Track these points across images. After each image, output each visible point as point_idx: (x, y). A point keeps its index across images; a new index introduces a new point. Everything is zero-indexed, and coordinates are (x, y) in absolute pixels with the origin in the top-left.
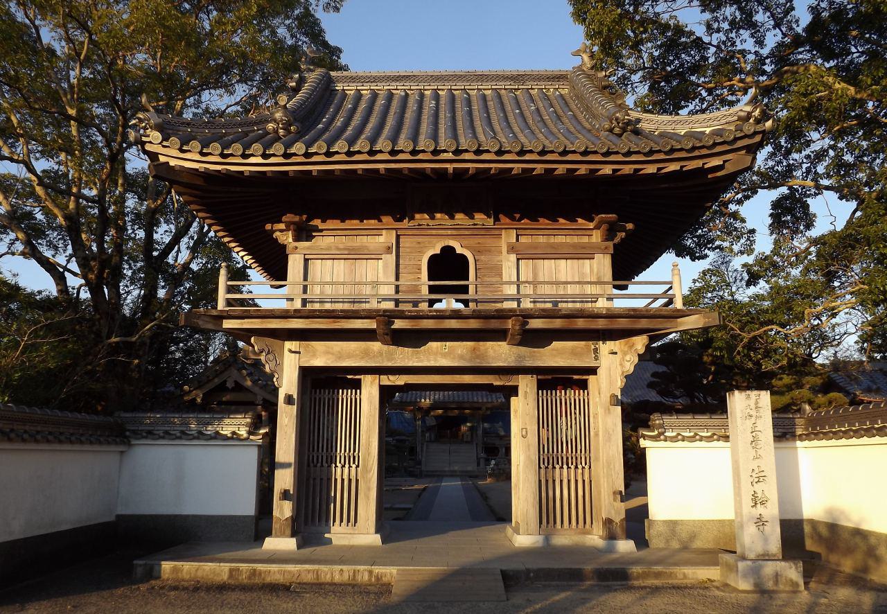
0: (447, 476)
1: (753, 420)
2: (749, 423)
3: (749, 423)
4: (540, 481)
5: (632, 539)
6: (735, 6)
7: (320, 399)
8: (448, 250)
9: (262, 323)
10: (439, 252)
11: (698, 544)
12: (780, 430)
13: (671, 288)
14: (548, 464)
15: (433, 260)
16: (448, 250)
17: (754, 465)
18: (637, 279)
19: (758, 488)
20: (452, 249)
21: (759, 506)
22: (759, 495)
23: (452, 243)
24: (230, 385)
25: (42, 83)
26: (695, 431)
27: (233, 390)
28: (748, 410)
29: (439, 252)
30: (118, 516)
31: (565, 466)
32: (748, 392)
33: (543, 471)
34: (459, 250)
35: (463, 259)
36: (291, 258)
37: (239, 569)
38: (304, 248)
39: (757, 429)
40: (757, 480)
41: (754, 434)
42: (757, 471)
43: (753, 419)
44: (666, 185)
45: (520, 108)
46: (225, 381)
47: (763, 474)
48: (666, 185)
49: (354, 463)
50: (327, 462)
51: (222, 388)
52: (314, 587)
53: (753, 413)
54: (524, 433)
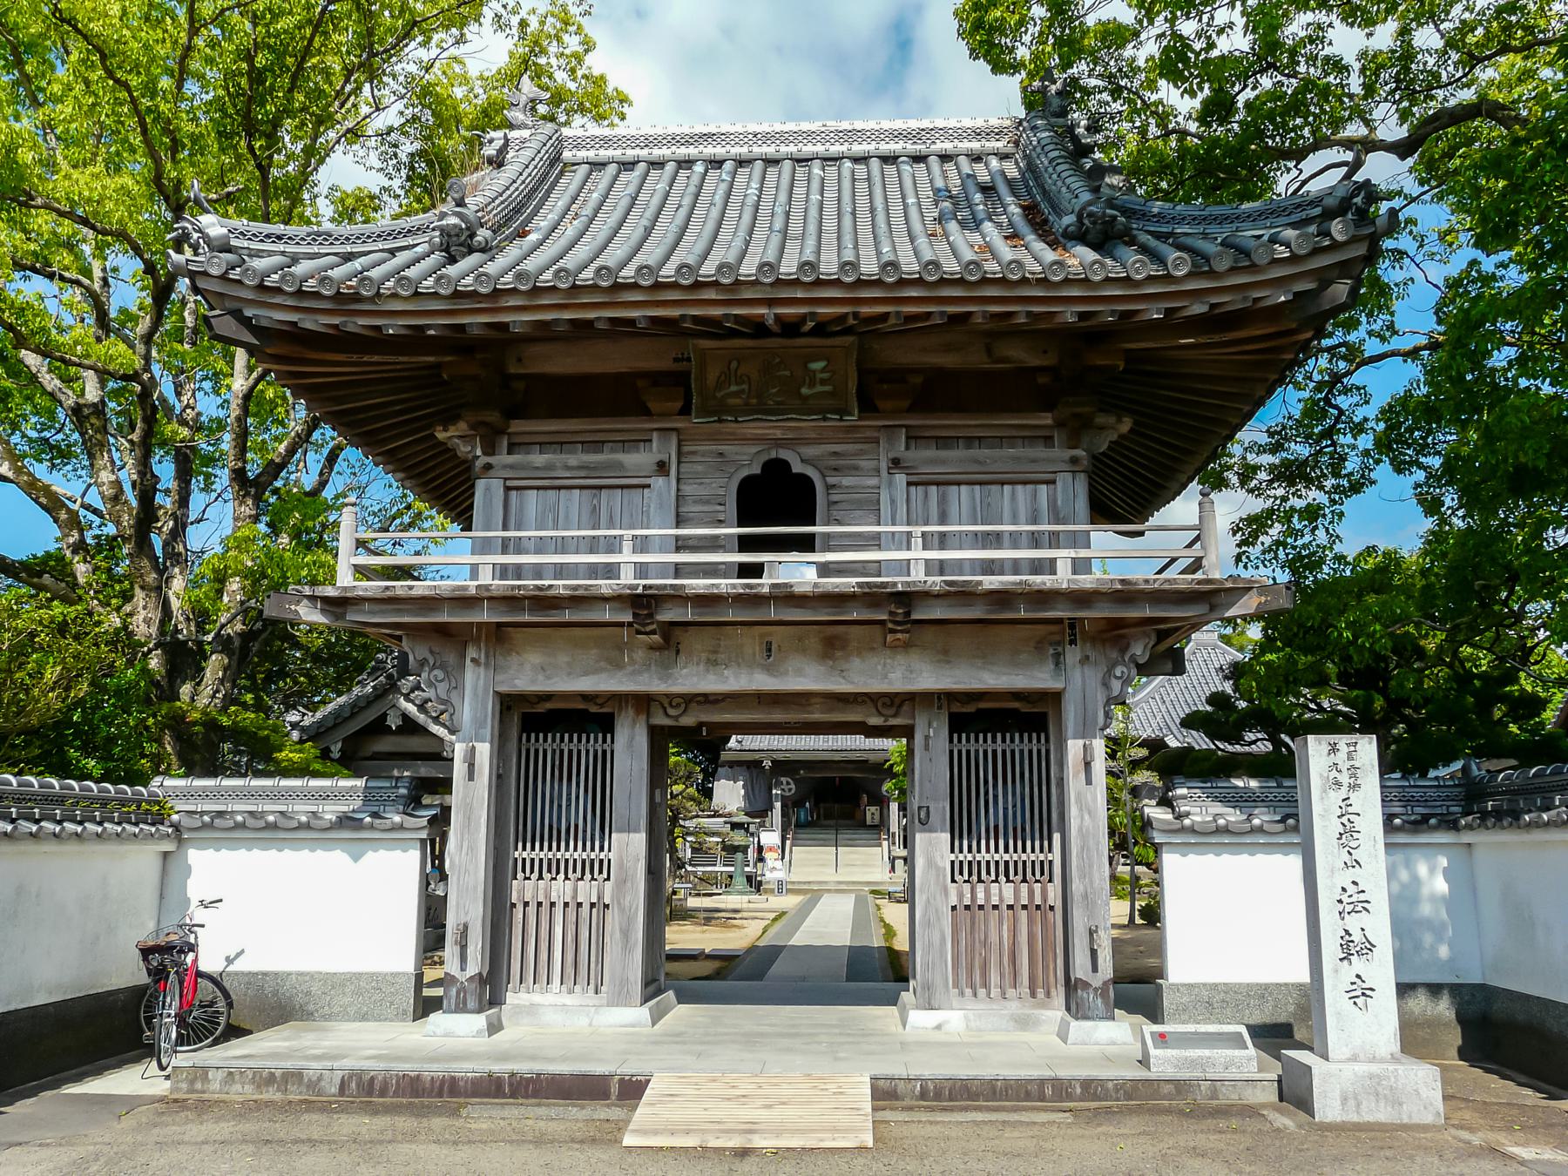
0: (829, 891)
1: (1343, 793)
2: (1336, 797)
3: (1336, 797)
7: (570, 752)
9: (717, 586)
10: (758, 471)
12: (1418, 810)
13: (1198, 538)
14: (970, 874)
17: (1345, 878)
18: (1157, 519)
19: (1353, 923)
20: (785, 465)
21: (1354, 958)
22: (1357, 937)
23: (785, 454)
24: (393, 722)
27: (401, 730)
28: (1334, 773)
29: (758, 471)
32: (1333, 738)
34: (797, 468)
35: (806, 482)
36: (480, 485)
37: (301, 1075)
39: (1350, 810)
40: (1349, 908)
41: (1344, 820)
43: (1344, 789)
44: (431, 359)
45: (671, 186)
46: (385, 715)
47: (1362, 897)
48: (431, 359)
49: (601, 872)
50: (549, 871)
51: (379, 727)
54: (923, 815)
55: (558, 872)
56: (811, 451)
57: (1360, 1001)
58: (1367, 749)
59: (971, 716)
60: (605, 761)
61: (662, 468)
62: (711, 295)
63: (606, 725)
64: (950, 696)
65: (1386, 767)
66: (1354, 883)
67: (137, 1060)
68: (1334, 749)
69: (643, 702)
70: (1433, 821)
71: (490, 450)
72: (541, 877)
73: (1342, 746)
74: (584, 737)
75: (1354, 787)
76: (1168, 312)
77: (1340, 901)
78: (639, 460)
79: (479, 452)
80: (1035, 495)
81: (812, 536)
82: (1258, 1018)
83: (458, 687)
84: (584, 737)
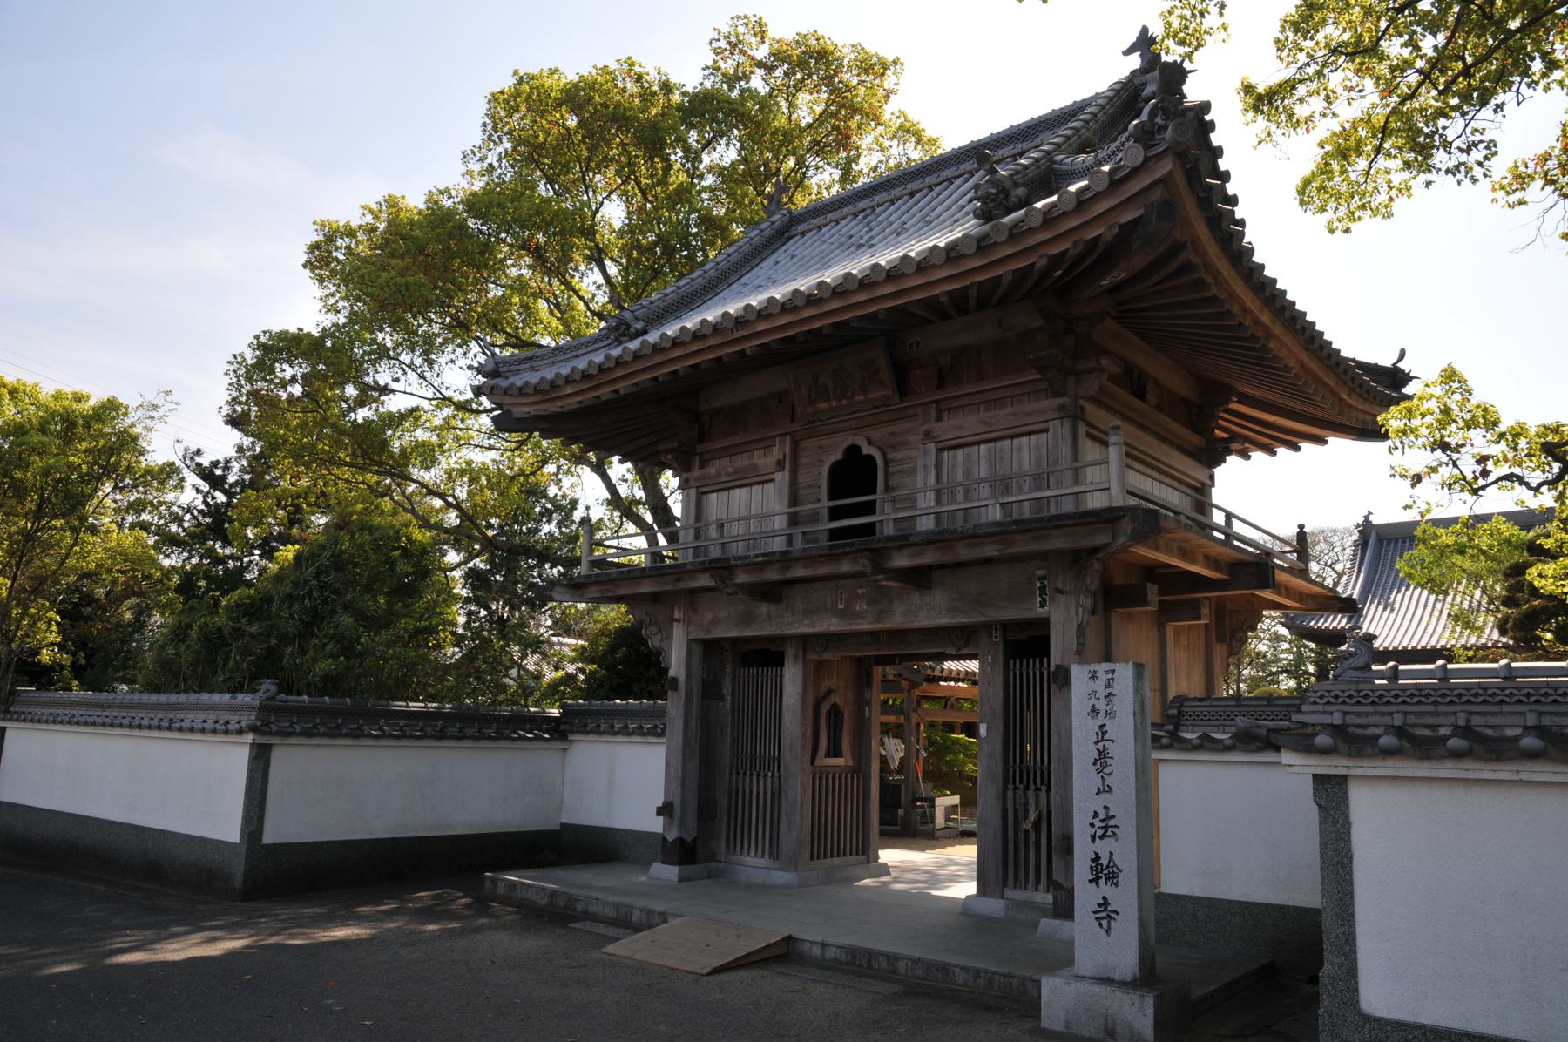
3: (1093, 725)
4: (1005, 811)
5: (1368, 1019)
6: (629, 465)
8: (853, 451)
11: (1197, 993)
15: (836, 469)
16: (853, 451)
17: (1097, 804)
19: (1103, 847)
21: (1102, 881)
22: (1104, 861)
25: (677, 214)
26: (1205, 729)
28: (1093, 701)
30: (563, 825)
31: (1032, 787)
33: (1010, 794)
35: (871, 458)
38: (697, 479)
40: (1100, 832)
42: (1102, 816)
52: (126, 722)
53: (1102, 705)
56: (876, 434)
57: (1104, 922)
61: (780, 465)
62: (677, 353)
63: (777, 660)
64: (1006, 626)
66: (1106, 807)
67: (1177, 898)
68: (1094, 677)
69: (805, 641)
73: (1103, 677)
75: (1110, 714)
77: (1092, 825)
83: (669, 637)
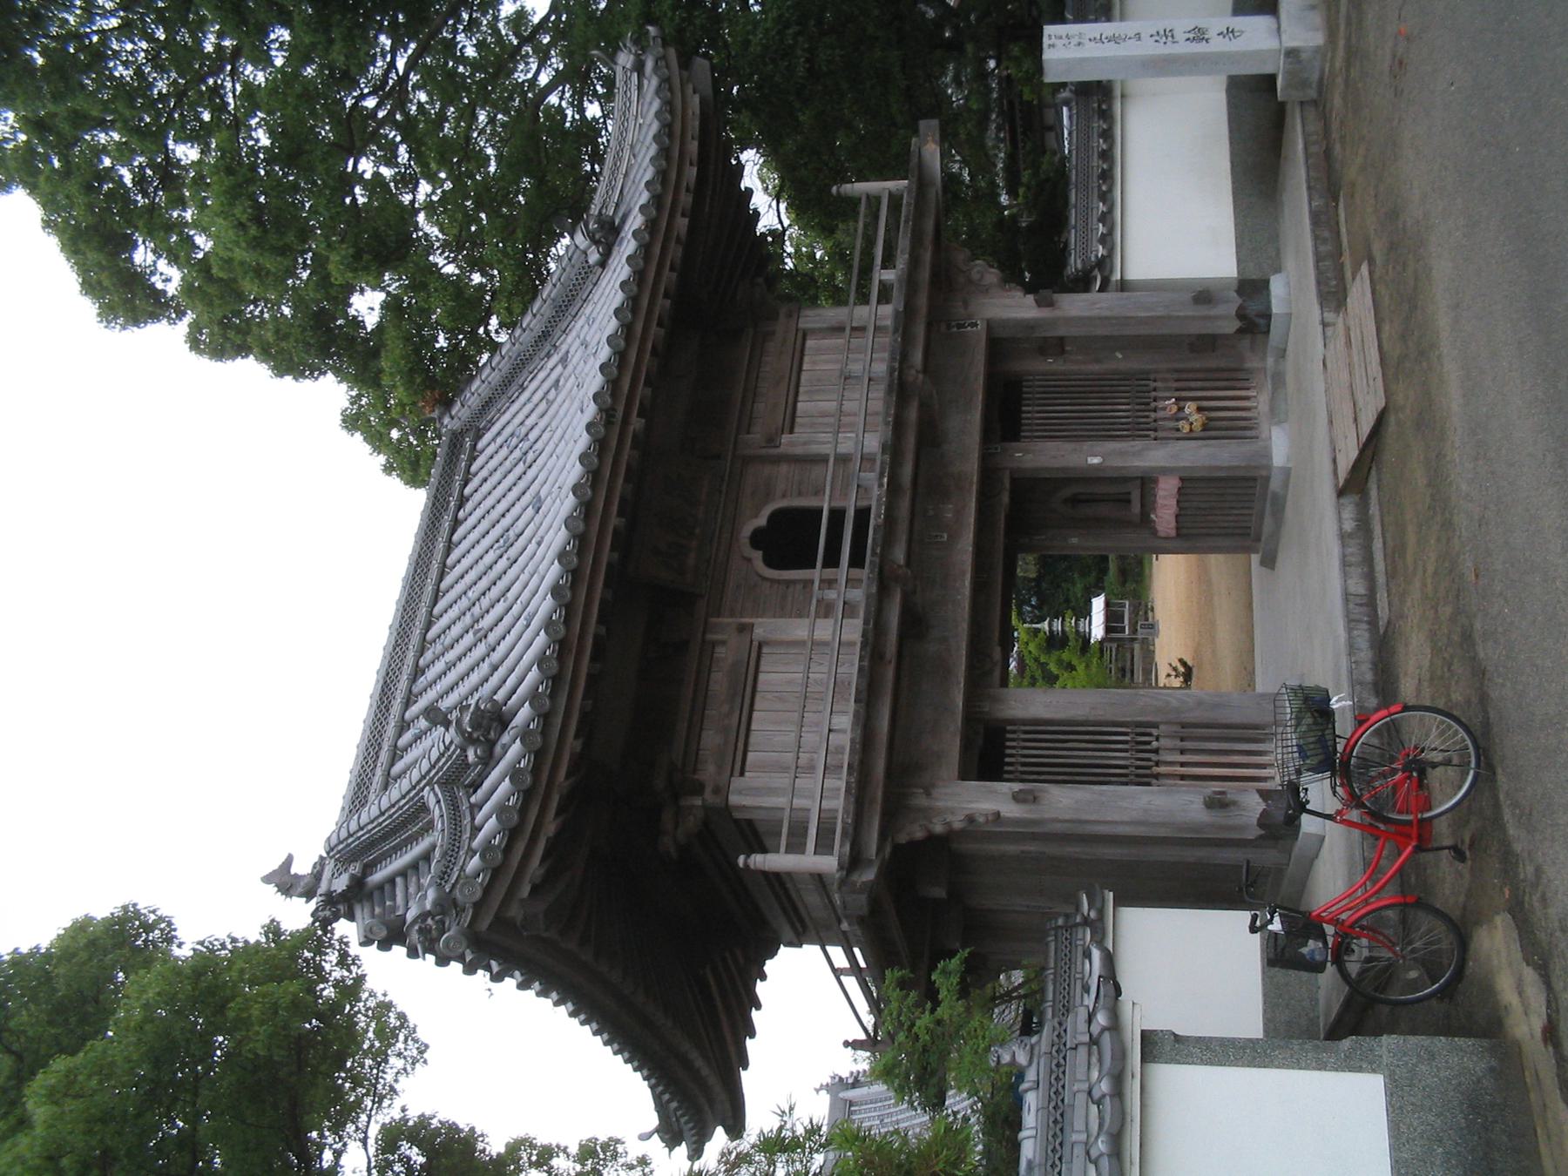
10: (760, 553)
29: (760, 553)
32: (1045, 46)
34: (762, 521)
35: (776, 517)
36: (734, 799)
55: (1150, 735)
58: (1049, 30)
59: (1006, 416)
60: (1038, 726)
65: (1063, 21)
70: (1104, 188)
71: (699, 789)
72: (1156, 751)
74: (1008, 751)
76: (666, 296)
78: (728, 652)
79: (698, 802)
80: (802, 425)
81: (832, 512)
82: (1293, 473)
84: (1008, 751)
